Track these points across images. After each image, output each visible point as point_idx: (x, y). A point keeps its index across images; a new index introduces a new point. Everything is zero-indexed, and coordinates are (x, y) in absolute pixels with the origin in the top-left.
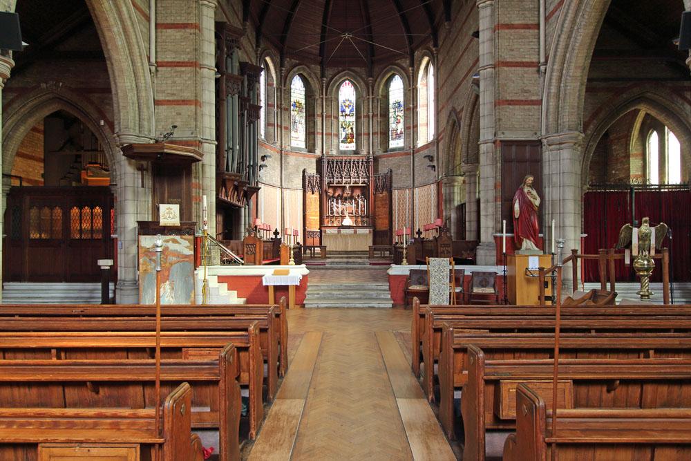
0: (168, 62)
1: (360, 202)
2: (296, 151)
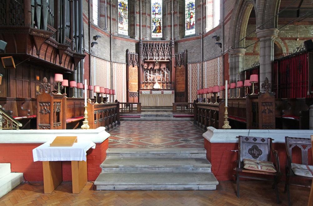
1: (166, 73)
2: (122, 37)
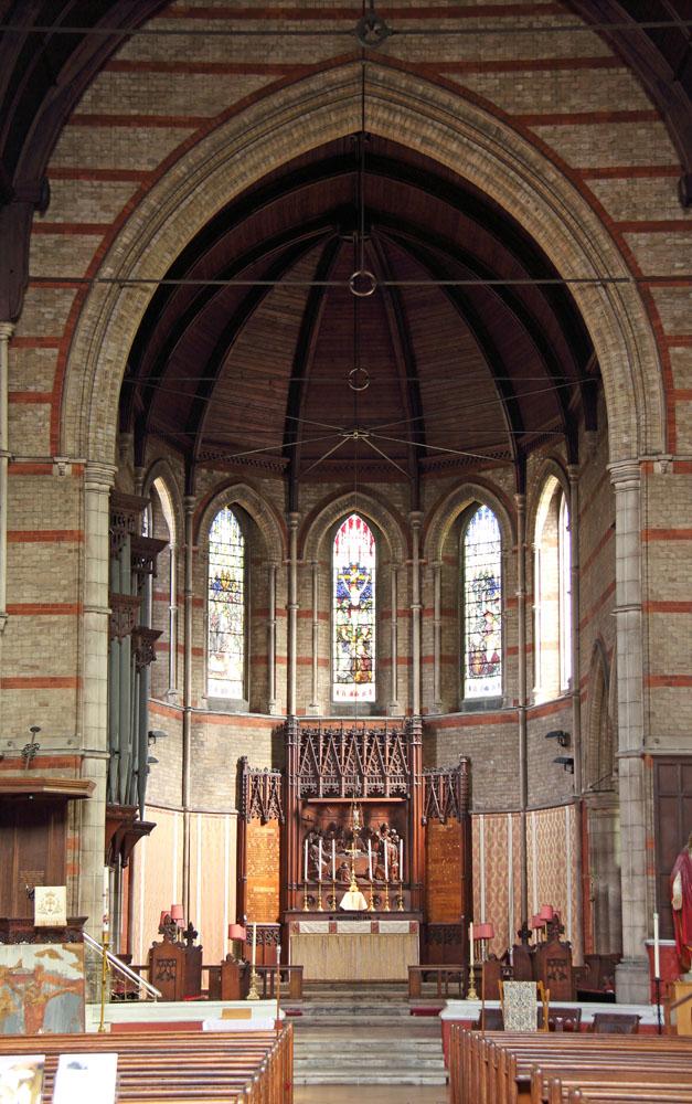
0: (24, 605)
1: (388, 846)
2: (220, 708)
